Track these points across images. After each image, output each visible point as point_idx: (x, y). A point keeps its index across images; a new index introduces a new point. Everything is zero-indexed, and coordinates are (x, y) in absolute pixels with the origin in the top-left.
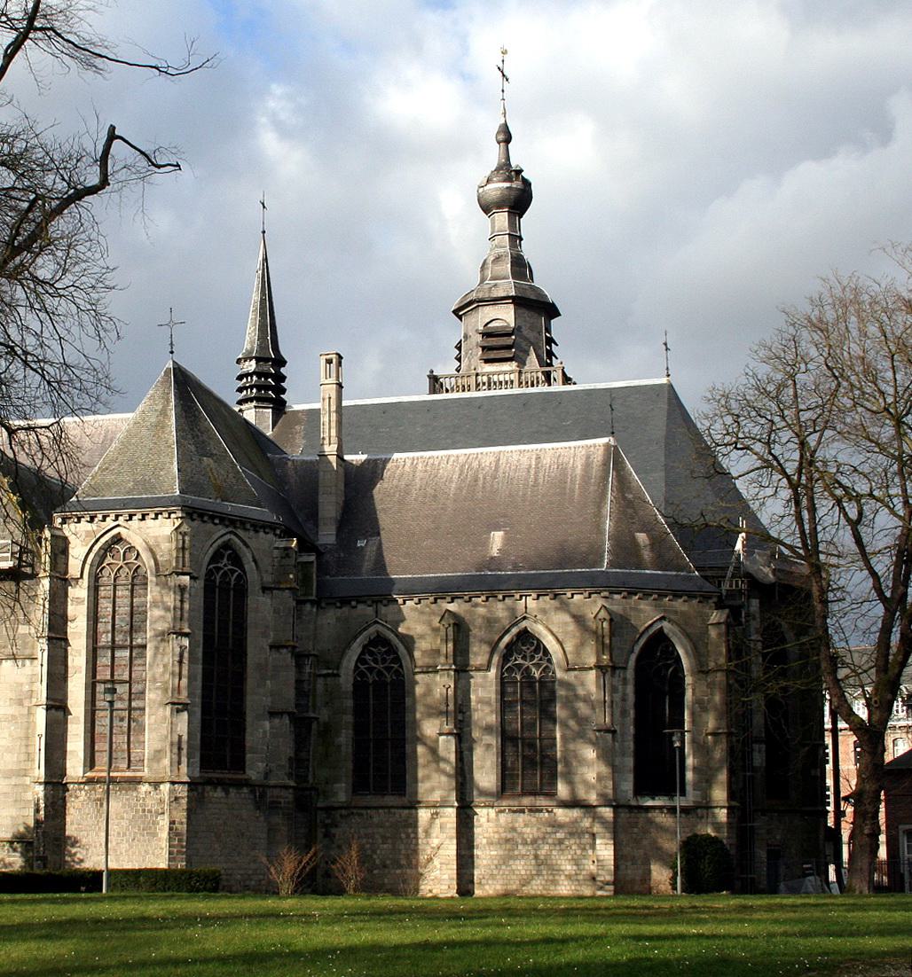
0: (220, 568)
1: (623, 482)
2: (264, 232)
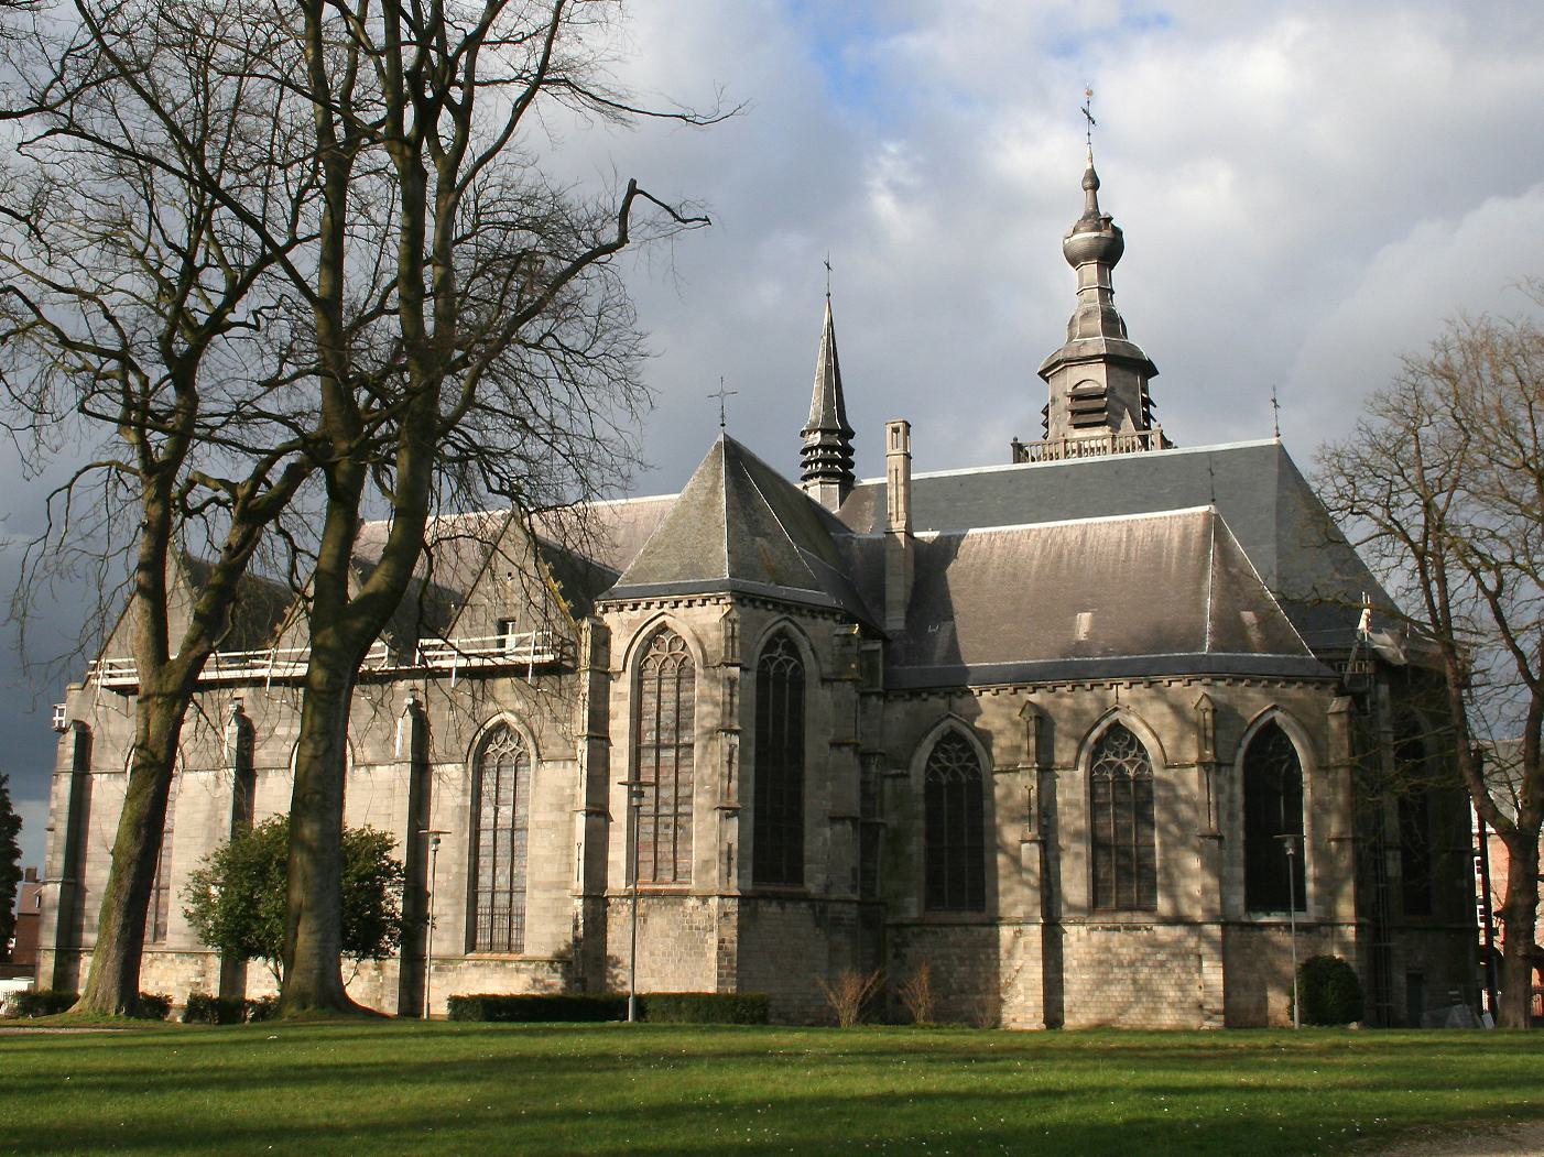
1: (1226, 554)
2: (829, 295)
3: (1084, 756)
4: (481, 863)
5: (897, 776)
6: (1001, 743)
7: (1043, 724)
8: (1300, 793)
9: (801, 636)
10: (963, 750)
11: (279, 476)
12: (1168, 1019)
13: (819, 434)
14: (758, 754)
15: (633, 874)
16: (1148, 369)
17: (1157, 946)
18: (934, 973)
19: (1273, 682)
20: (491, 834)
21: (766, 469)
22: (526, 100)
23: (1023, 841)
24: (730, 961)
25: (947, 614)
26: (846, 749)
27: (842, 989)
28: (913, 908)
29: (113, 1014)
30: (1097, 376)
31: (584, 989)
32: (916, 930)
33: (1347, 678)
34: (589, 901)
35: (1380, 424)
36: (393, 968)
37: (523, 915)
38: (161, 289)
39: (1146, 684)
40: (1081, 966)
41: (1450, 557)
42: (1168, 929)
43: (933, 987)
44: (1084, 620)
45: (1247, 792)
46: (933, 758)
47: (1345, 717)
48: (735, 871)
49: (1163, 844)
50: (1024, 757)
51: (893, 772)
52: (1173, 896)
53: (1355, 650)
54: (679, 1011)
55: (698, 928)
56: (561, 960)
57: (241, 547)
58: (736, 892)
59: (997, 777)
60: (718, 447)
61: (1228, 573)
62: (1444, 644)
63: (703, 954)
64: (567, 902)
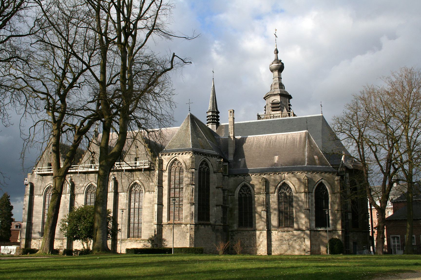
1: (310, 142)
3: (277, 190)
4: (131, 217)
5: (231, 195)
6: (257, 187)
7: (267, 183)
8: (328, 199)
9: (209, 162)
11: (86, 124)
12: (297, 253)
13: (211, 113)
14: (199, 190)
15: (169, 219)
16: (290, 97)
17: (294, 236)
18: (241, 242)
19: (322, 173)
20: (133, 209)
21: (199, 121)
22: (149, 34)
23: (262, 211)
24: (193, 240)
25: (243, 156)
26: (220, 189)
27: (219, 246)
28: (235, 227)
29: (48, 254)
30: (278, 99)
31: (157, 247)
32: (236, 232)
33: (339, 172)
34: (158, 226)
35: (348, 111)
36: (109, 242)
37: (141, 229)
38: (56, 77)
39: (291, 173)
40: (276, 240)
41: (364, 142)
42: (297, 232)
43: (241, 246)
44: (276, 158)
45: (315, 199)
46: (240, 191)
47: (339, 181)
48: (193, 218)
49: (295, 211)
50: (262, 191)
51: (231, 194)
52: (298, 224)
53: (341, 165)
54: (181, 252)
55: (185, 232)
56: (151, 240)
57: (77, 141)
58: (194, 223)
59: (256, 195)
60: (188, 116)
61: (311, 147)
62: (363, 164)
63: (186, 238)
64: (152, 226)
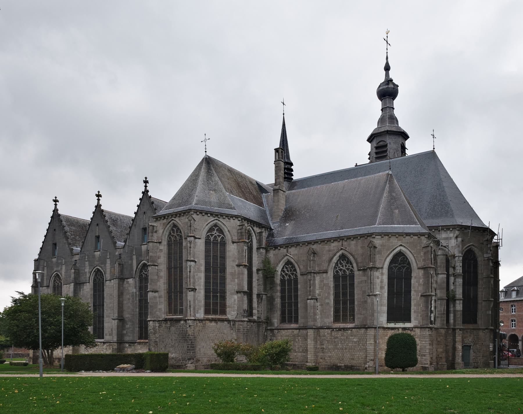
0: (213, 235)
1: (392, 190)
2: (284, 114)
10: (292, 267)
